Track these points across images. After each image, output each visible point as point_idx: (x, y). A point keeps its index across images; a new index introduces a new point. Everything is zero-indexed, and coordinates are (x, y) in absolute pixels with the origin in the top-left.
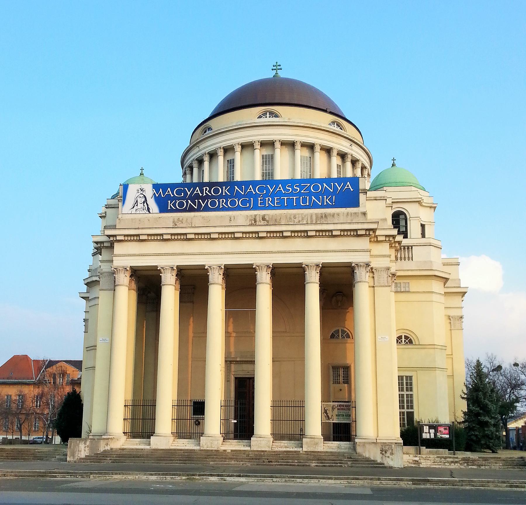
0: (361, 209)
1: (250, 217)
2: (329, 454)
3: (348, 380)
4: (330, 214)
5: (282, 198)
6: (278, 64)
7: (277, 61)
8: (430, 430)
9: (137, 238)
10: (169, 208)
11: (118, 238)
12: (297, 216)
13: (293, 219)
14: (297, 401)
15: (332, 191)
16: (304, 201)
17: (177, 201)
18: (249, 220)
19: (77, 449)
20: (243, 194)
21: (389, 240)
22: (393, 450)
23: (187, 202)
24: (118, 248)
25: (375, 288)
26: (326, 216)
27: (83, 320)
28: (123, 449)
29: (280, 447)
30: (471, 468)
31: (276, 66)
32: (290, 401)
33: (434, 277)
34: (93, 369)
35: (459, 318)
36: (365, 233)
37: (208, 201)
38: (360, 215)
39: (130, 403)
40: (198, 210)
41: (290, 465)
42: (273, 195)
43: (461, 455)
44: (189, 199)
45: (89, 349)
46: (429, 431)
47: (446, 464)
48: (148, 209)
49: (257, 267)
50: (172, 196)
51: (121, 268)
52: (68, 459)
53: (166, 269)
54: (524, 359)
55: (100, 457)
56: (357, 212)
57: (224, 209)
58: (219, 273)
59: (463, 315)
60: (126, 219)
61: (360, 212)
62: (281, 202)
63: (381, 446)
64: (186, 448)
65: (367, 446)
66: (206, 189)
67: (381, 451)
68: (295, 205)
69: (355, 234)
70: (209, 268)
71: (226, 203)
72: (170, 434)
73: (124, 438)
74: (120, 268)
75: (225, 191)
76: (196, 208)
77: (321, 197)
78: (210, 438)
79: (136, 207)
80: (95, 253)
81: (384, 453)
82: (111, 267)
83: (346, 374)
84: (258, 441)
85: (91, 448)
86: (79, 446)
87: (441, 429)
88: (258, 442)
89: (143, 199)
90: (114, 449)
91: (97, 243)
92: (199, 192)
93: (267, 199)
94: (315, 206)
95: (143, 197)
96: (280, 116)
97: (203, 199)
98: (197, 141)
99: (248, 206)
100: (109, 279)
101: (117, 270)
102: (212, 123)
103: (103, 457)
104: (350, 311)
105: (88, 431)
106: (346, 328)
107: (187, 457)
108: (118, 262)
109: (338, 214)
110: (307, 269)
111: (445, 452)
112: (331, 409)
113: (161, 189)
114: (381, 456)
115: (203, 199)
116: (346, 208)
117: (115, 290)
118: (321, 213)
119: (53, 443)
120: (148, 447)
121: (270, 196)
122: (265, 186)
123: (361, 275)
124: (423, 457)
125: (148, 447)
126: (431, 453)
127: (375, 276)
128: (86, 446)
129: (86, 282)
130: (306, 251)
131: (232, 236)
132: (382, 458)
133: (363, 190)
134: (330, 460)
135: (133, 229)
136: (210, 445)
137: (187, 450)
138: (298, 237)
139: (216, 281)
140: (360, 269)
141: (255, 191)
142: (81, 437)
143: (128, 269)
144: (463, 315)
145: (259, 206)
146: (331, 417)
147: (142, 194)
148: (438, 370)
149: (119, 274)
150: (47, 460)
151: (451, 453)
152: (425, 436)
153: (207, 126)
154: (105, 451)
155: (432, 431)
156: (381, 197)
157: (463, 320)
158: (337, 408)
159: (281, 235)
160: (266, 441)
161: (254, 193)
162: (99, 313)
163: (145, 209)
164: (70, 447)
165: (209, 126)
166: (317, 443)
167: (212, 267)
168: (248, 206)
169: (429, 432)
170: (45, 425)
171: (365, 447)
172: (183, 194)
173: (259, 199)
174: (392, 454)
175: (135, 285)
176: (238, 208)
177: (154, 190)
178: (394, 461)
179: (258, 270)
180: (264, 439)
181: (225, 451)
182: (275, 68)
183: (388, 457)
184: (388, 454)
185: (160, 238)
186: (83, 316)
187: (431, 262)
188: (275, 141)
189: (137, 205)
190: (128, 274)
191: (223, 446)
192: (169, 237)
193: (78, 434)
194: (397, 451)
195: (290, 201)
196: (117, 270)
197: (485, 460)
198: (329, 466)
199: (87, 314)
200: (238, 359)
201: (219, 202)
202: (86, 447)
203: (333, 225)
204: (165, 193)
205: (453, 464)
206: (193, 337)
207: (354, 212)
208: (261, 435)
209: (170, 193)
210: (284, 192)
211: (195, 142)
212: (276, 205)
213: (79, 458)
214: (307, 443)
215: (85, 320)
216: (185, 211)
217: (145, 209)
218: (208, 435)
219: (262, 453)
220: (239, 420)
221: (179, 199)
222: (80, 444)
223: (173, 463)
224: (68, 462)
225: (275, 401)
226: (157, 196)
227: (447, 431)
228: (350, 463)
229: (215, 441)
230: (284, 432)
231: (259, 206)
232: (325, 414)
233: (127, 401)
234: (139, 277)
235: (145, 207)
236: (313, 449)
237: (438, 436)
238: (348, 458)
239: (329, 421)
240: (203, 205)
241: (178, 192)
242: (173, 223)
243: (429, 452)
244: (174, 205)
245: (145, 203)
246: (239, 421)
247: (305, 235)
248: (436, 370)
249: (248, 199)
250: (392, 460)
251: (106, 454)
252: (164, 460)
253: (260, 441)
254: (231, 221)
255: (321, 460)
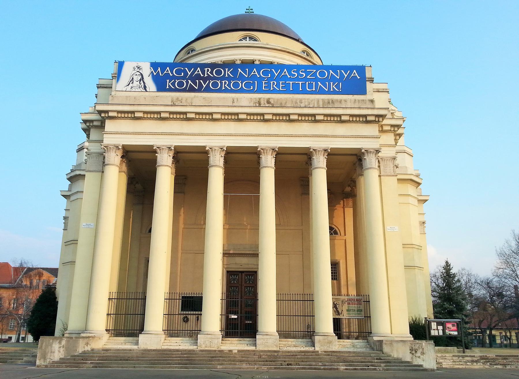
0: (368, 97)
1: (255, 100)
2: (354, 355)
3: (336, 276)
4: (337, 100)
5: (287, 82)
6: (251, 8)
7: (250, 6)
8: (438, 326)
9: (131, 116)
10: (168, 87)
11: (111, 114)
12: (303, 100)
13: (299, 103)
14: (306, 294)
15: (338, 78)
16: (310, 86)
17: (176, 80)
18: (253, 103)
19: (50, 350)
20: (247, 76)
21: (394, 130)
22: (423, 349)
23: (187, 82)
24: (109, 125)
25: (381, 177)
26: (333, 102)
27: (63, 218)
28: (107, 350)
29: (288, 346)
30: (496, 368)
31: (248, 10)
32: (296, 294)
33: (410, 181)
34: (71, 264)
35: (422, 223)
36: (374, 119)
37: (209, 82)
38: (368, 102)
39: (114, 296)
40: (199, 90)
41: (315, 369)
42: (278, 79)
43: (477, 352)
44: (189, 78)
45: (67, 244)
46: (437, 327)
47: (468, 364)
48: (145, 87)
49: (262, 150)
50: (171, 75)
51: (113, 147)
52: (38, 362)
53: (163, 149)
54: (435, 270)
55: (79, 360)
56: (365, 99)
57: (226, 91)
58: (221, 155)
59: (426, 221)
60: (120, 96)
61: (367, 99)
62: (287, 86)
63: (409, 344)
64: (181, 348)
65: (395, 344)
66: (208, 70)
67: (410, 350)
68: (301, 89)
69: (364, 120)
70: (209, 149)
71: (229, 85)
72: (161, 332)
73: (106, 336)
74: (110, 146)
75: (228, 72)
76: (197, 88)
77: (327, 83)
78: (209, 336)
79: (131, 85)
80: (80, 149)
81: (414, 352)
82: (101, 145)
83: (334, 270)
84: (264, 339)
85: (67, 349)
86: (51, 347)
87: (449, 325)
88: (264, 340)
89: (140, 77)
90: (96, 349)
91: (85, 121)
92: (200, 72)
93: (272, 82)
94: (321, 92)
95: (139, 75)
96: (258, 39)
97: (205, 79)
98: (181, 60)
99: (252, 88)
100: (98, 160)
101: (107, 149)
102: (195, 45)
103: (82, 360)
104: (337, 209)
105: (62, 329)
106: (334, 225)
107: (187, 360)
108: (108, 140)
109: (345, 101)
110: (315, 154)
111: (454, 350)
112: (340, 302)
113: (159, 68)
114: (410, 356)
115: (205, 79)
116: (353, 95)
117: (103, 172)
118: (328, 99)
119: (26, 342)
120: (135, 347)
121: (275, 80)
122: (270, 70)
123: (370, 161)
124: (438, 356)
125: (135, 347)
126: (440, 352)
127: (381, 165)
128: (61, 346)
129: (69, 176)
130: (314, 136)
131: (235, 117)
132: (412, 358)
133: (370, 78)
134: (358, 362)
135: (128, 105)
136: (208, 345)
137: (186, 350)
138: (305, 121)
139: (217, 163)
140: (369, 156)
141: (259, 74)
142: (54, 336)
143: (120, 147)
144: (426, 221)
145: (264, 89)
146: (341, 312)
147: (139, 72)
148: (417, 269)
149: (109, 153)
150: (12, 363)
151: (460, 352)
152: (434, 333)
153: (191, 48)
154: (84, 352)
155: (441, 328)
156: (383, 89)
157: (425, 225)
158: (347, 302)
159: (287, 119)
160: (273, 339)
161: (258, 76)
162: (82, 206)
163: (141, 87)
164: (41, 347)
165: (193, 48)
166: (331, 342)
167: (213, 149)
168: (252, 88)
169: (437, 329)
170: (18, 324)
171: (393, 345)
172: (183, 73)
173: (264, 82)
174: (423, 353)
175: (126, 168)
176: (242, 91)
177: (152, 68)
178: (426, 362)
179: (263, 153)
180: (271, 337)
181: (230, 351)
182: (248, 11)
183: (419, 357)
184: (419, 354)
185: (157, 116)
186: (64, 213)
187: (406, 167)
188: (255, 60)
189: (133, 83)
190: (120, 153)
191: (224, 345)
192: (167, 115)
193: (51, 332)
194: (428, 350)
195: (296, 86)
196: (107, 149)
197: (505, 359)
198: (361, 369)
199: (68, 212)
200: (231, 252)
201: (221, 83)
202: (61, 347)
203: (342, 110)
204: (164, 72)
205: (475, 364)
206: (183, 228)
207: (361, 99)
208: (267, 332)
209: (169, 72)
210: (289, 77)
211: (180, 61)
212: (281, 89)
213: (51, 361)
214: (320, 341)
215: (65, 218)
216: (184, 90)
217: (141, 87)
218: (206, 333)
219: (276, 354)
220: (239, 315)
221: (178, 78)
222: (54, 343)
223: (171, 367)
224: (38, 367)
225: (279, 294)
226: (155, 74)
227: (455, 328)
228: (383, 365)
229: (214, 340)
230: (297, 328)
231: (264, 89)
232: (334, 308)
233: (111, 294)
234: (130, 161)
235: (141, 85)
236: (327, 348)
237: (447, 333)
238: (377, 359)
239: (338, 316)
240: (204, 86)
241: (178, 72)
242: (171, 102)
243: (437, 351)
244: (173, 84)
245: (142, 81)
246: (240, 317)
247: (313, 119)
248: (415, 269)
249: (252, 82)
250: (424, 361)
251: (85, 356)
252: (160, 364)
253: (267, 339)
254: (234, 102)
255: (347, 362)
